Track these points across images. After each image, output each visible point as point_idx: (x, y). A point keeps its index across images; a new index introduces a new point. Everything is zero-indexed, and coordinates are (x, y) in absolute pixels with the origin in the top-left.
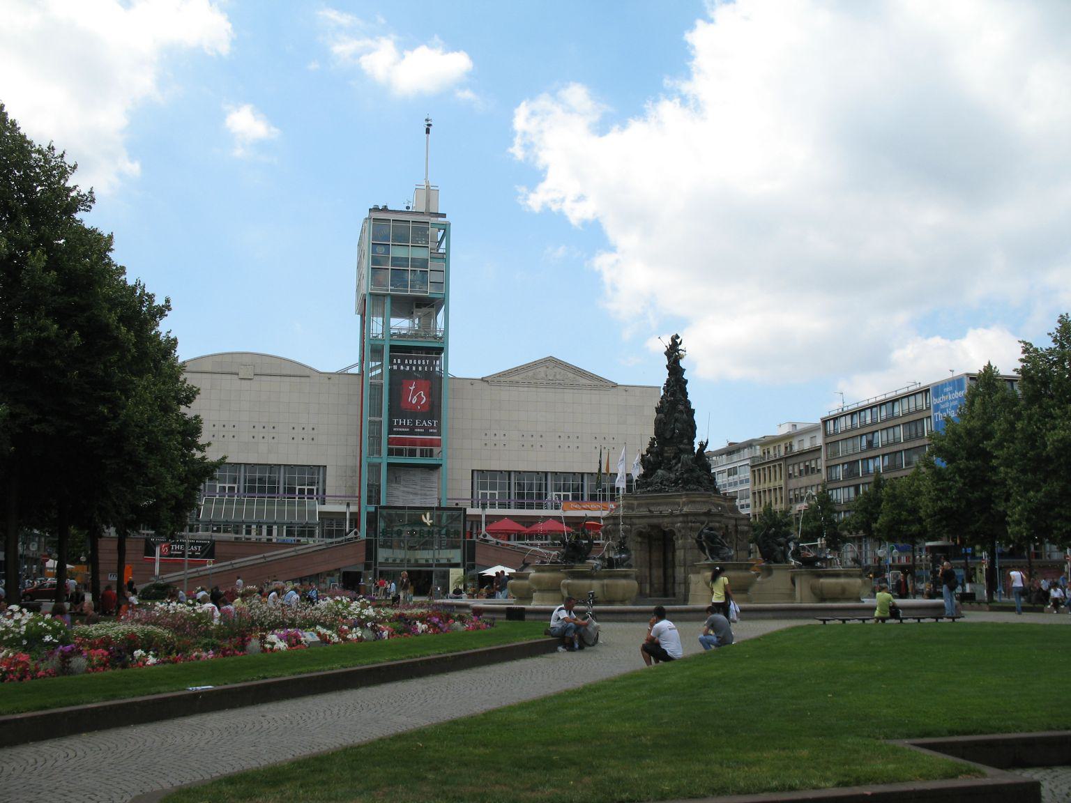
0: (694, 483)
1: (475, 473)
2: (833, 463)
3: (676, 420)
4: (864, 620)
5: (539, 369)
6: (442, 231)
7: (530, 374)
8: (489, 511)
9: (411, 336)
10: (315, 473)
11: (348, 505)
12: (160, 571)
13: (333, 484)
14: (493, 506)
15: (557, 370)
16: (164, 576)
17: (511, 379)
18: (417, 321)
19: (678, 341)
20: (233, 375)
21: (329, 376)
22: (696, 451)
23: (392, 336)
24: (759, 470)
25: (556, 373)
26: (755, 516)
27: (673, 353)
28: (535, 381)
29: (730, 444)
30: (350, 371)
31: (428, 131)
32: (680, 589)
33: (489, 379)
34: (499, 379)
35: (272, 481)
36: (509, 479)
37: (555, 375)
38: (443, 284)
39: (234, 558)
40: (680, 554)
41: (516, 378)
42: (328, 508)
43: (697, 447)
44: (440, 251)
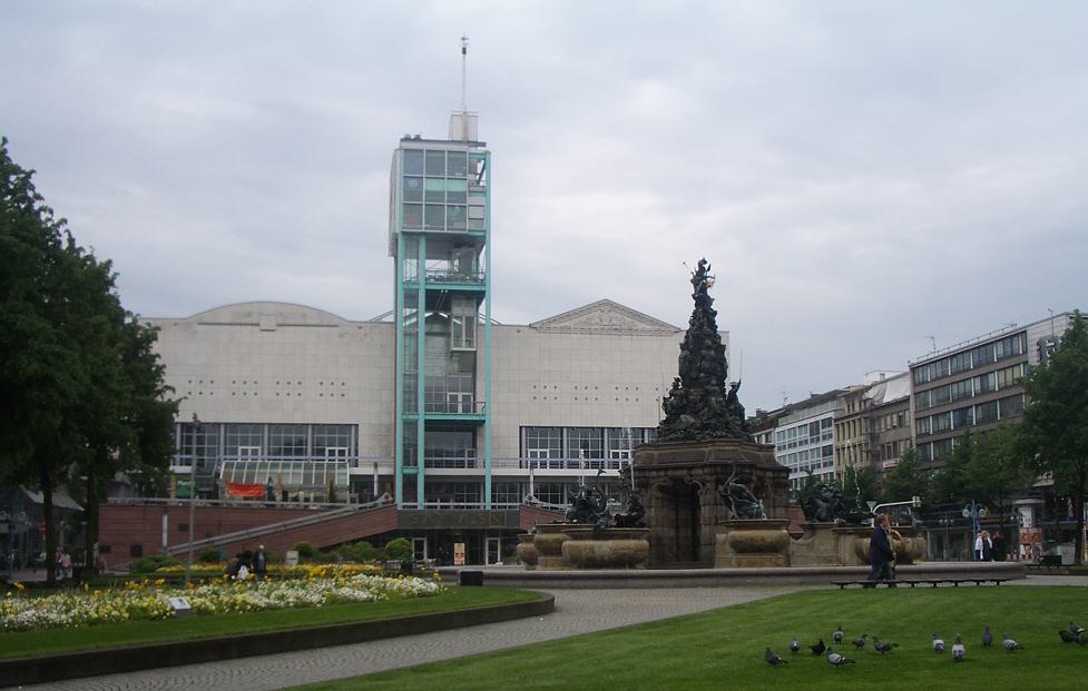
0: (723, 430)
1: (524, 430)
2: (922, 415)
3: (703, 358)
4: (998, 581)
6: (483, 162)
7: (584, 318)
8: (539, 472)
9: (449, 279)
10: (343, 433)
11: (376, 465)
12: (168, 541)
13: (367, 444)
14: (543, 465)
16: (174, 548)
17: (562, 325)
18: (456, 262)
19: (706, 266)
21: (360, 325)
22: (727, 393)
23: (426, 279)
24: (843, 424)
26: (839, 475)
27: (701, 280)
29: (813, 396)
30: (384, 320)
31: (464, 51)
32: (704, 551)
35: (300, 442)
36: (562, 436)
38: (483, 220)
39: (251, 527)
40: (705, 511)
42: (359, 471)
43: (728, 388)
44: (481, 184)
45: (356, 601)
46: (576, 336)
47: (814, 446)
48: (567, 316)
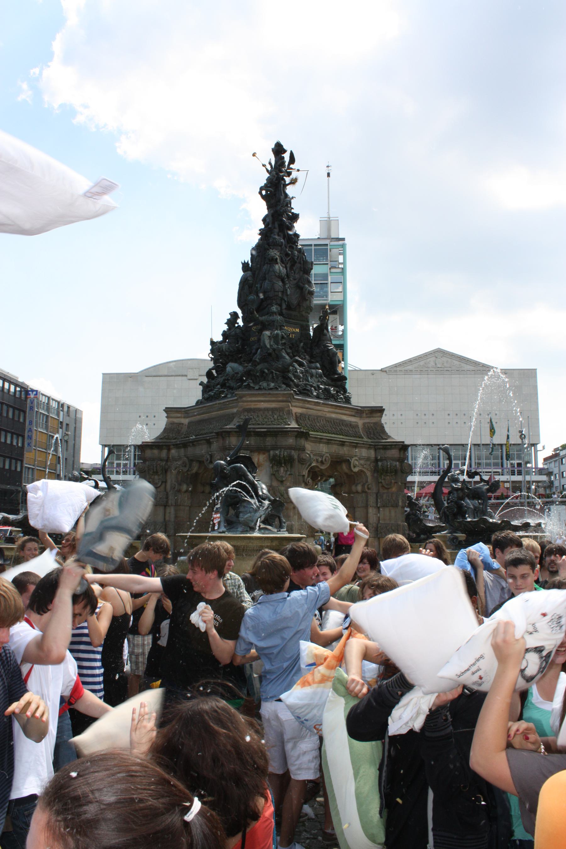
5: (429, 360)
7: (422, 363)
15: (445, 359)
20: (183, 377)
25: (444, 361)
28: (426, 369)
31: (329, 175)
33: (387, 370)
34: (395, 369)
37: (443, 364)
41: (410, 367)
46: (416, 376)
48: (410, 361)
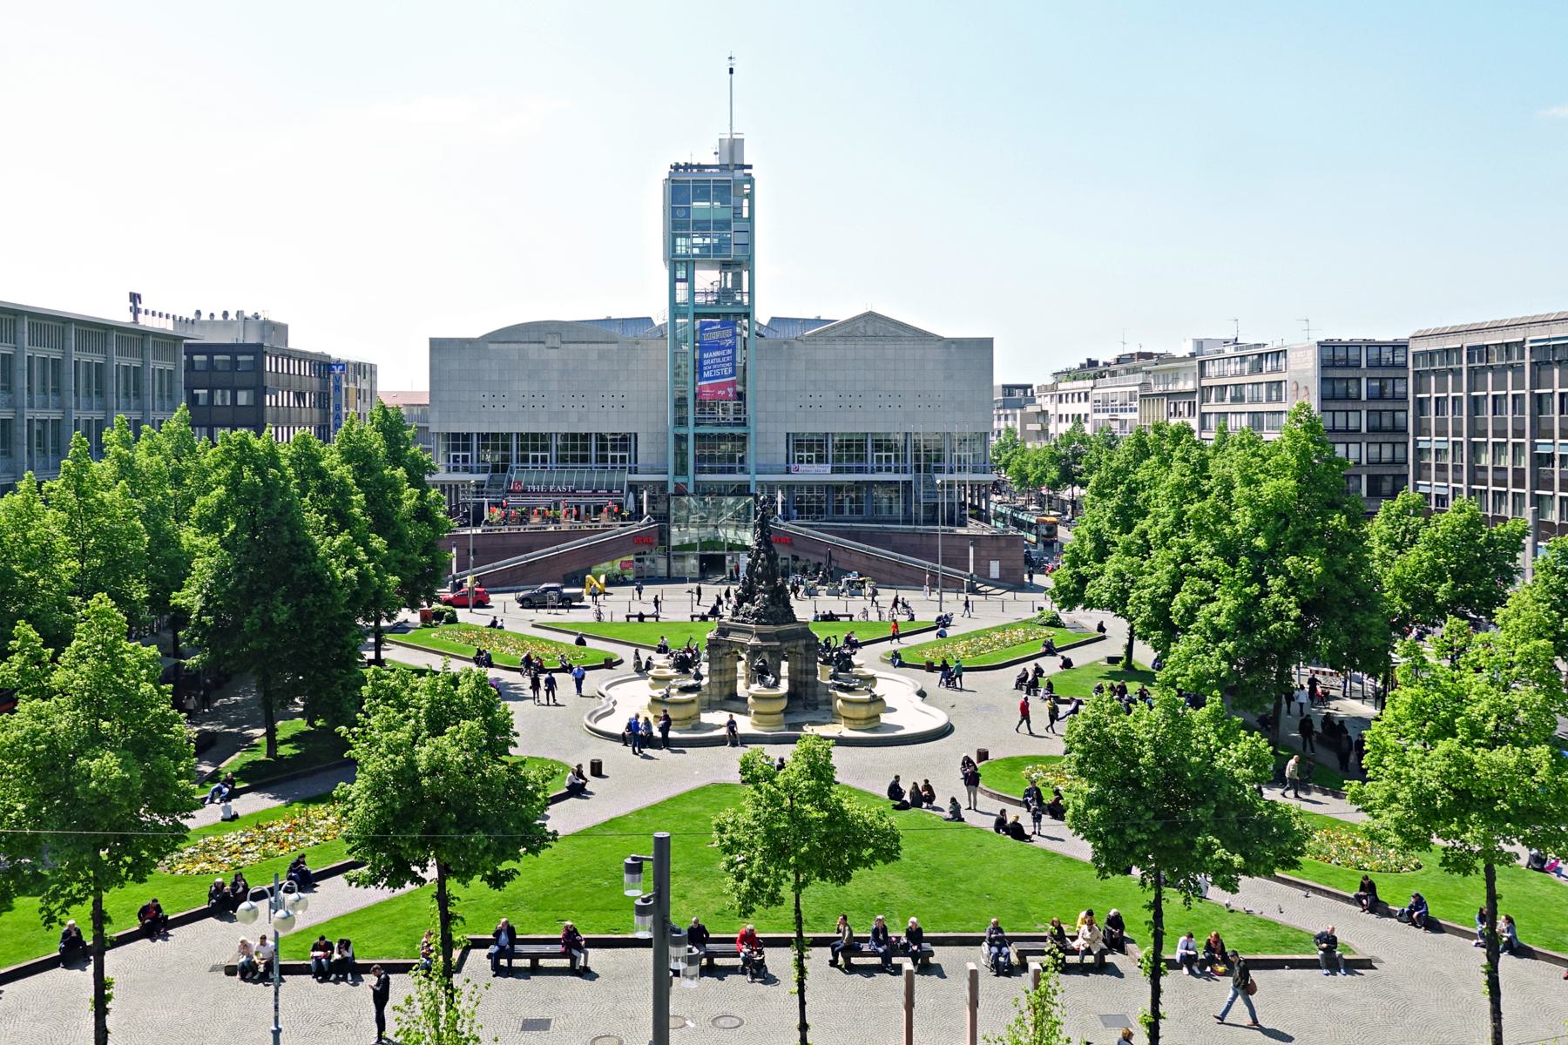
10: (624, 441)
31: (731, 71)
45: (651, 747)
47: (956, 477)
